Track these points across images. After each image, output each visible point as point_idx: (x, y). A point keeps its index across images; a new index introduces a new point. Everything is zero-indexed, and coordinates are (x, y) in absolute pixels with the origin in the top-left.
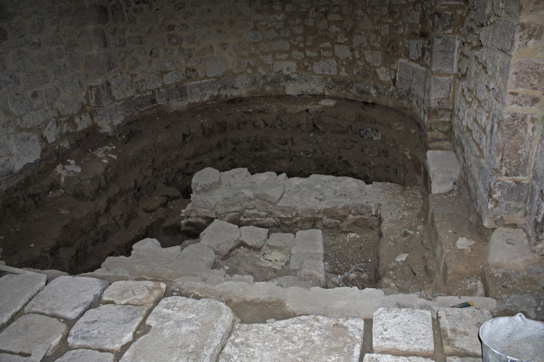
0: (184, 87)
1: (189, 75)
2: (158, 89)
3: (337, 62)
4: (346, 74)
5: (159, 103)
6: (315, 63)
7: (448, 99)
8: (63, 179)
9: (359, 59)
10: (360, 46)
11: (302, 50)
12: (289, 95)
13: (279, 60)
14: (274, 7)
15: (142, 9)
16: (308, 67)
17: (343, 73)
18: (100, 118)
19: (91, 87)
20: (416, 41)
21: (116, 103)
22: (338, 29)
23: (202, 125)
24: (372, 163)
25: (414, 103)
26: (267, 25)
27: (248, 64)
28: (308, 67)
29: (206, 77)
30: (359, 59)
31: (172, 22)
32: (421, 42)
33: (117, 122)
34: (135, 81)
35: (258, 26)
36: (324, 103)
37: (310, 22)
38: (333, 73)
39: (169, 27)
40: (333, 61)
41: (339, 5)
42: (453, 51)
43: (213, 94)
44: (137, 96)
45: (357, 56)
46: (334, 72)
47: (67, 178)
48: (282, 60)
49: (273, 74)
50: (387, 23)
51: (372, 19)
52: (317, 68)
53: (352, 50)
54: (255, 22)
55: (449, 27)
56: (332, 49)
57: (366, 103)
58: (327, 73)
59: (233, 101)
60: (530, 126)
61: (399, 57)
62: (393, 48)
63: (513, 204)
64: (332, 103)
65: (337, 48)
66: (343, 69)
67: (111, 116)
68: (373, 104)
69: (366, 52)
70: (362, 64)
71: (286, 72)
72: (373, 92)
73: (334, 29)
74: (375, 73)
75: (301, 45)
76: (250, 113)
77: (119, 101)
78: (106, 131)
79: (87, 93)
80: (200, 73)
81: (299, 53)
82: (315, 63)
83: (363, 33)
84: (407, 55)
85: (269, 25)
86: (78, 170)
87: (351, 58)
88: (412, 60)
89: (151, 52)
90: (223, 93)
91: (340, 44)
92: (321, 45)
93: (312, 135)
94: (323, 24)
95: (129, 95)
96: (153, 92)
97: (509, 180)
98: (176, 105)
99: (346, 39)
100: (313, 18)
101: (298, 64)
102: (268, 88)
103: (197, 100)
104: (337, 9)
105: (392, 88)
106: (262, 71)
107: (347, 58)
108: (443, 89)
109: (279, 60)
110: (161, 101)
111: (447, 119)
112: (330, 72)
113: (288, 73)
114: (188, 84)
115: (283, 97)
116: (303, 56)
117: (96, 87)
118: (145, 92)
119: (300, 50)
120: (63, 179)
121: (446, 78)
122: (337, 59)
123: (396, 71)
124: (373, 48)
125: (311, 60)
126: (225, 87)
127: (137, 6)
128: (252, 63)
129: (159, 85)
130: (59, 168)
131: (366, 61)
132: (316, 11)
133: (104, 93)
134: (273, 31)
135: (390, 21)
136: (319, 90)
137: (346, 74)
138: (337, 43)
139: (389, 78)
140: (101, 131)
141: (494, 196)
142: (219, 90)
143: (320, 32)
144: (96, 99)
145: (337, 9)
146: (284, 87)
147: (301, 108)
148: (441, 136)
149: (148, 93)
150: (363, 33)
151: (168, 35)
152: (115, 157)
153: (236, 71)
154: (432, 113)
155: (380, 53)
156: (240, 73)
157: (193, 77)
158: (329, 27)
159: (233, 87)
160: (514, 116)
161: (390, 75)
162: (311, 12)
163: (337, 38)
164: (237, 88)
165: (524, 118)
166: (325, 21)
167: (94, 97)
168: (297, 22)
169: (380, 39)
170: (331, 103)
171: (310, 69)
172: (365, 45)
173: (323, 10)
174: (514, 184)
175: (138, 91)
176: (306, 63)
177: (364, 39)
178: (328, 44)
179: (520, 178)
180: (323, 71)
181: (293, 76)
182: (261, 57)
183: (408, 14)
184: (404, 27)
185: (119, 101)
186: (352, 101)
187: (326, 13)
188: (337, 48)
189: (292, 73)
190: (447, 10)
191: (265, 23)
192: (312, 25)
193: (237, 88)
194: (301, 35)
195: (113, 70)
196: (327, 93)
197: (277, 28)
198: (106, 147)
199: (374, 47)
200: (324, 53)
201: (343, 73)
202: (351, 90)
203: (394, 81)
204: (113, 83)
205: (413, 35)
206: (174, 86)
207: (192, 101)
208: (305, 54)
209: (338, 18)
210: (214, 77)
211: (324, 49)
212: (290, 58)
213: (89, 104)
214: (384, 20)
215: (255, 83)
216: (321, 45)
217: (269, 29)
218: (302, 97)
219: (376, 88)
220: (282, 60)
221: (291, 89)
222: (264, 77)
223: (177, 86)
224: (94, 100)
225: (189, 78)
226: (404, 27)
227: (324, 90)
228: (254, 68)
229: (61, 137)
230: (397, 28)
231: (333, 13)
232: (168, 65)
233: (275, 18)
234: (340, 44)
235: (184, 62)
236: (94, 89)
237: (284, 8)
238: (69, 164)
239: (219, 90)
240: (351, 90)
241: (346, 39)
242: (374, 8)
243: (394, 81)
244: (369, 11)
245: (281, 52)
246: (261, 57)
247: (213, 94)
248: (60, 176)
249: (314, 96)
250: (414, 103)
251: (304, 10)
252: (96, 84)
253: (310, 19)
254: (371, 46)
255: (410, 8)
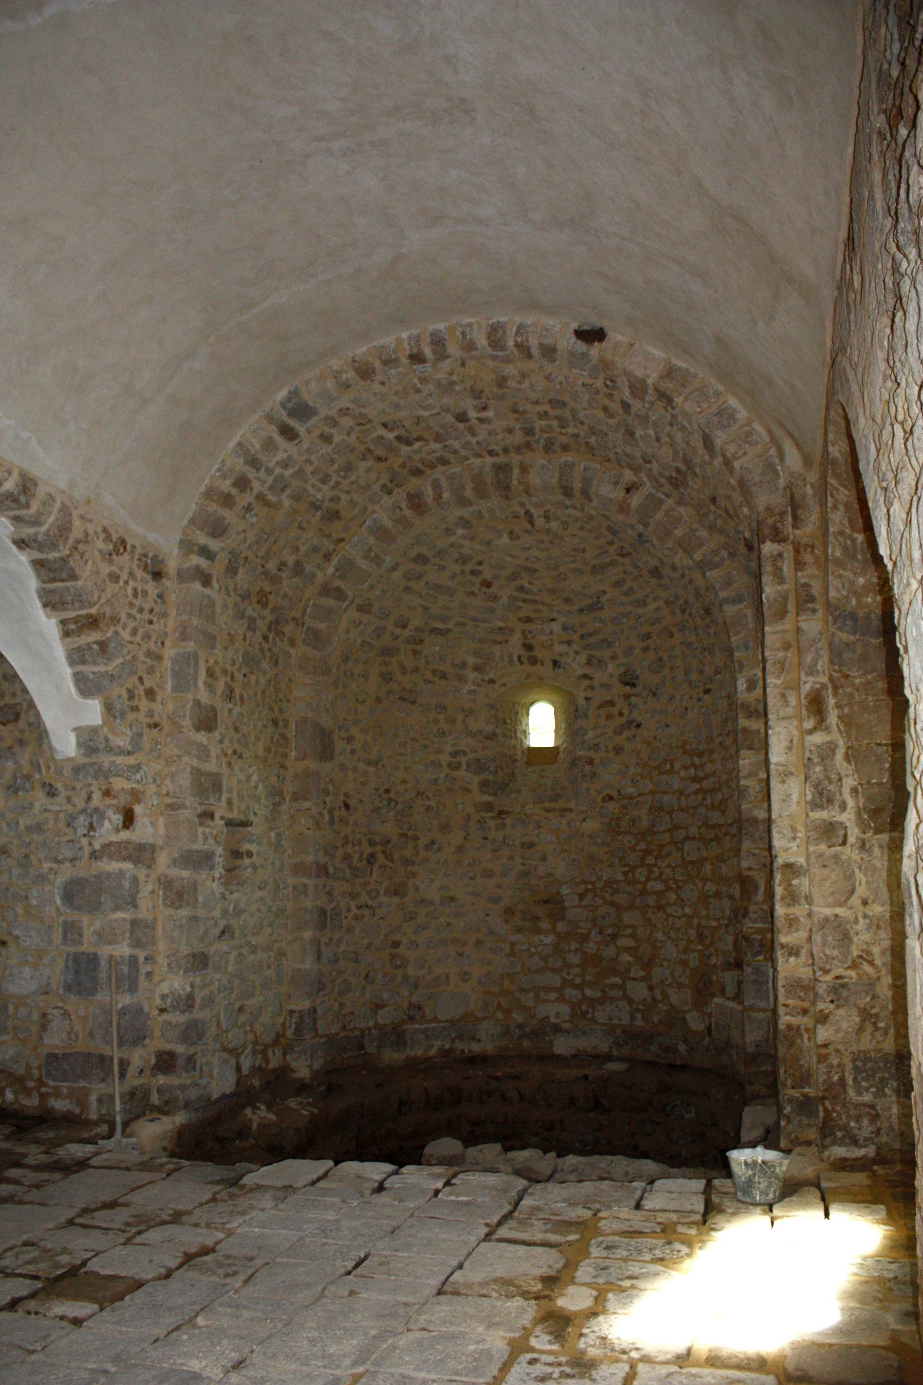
0: (405, 1031)
1: (412, 1013)
2: (369, 1029)
3: (630, 1006)
4: (643, 1024)
5: (368, 1050)
6: (598, 1007)
7: (767, 1041)
8: (255, 1125)
9: (661, 1001)
10: (662, 982)
11: (580, 987)
12: (558, 1056)
13: (545, 1001)
14: (540, 924)
15: (363, 916)
16: (587, 1012)
17: (639, 1022)
18: (295, 1056)
19: (292, 1012)
20: (731, 973)
21: (318, 1039)
22: (630, 959)
23: (426, 1090)
24: (684, 1153)
25: (735, 1057)
26: (529, 950)
27: (499, 1004)
28: (587, 1012)
29: (435, 1019)
30: (661, 1001)
31: (397, 937)
32: (736, 973)
33: (317, 1065)
34: (343, 1012)
35: (516, 950)
36: (610, 1066)
37: (591, 948)
38: (623, 1023)
39: (394, 942)
40: (624, 1004)
41: (632, 926)
42: (75, 610)
43: (443, 1046)
44: (342, 1034)
45: (659, 996)
46: (626, 1021)
47: (259, 1124)
48: (549, 1001)
49: (534, 1022)
50: (695, 951)
51: (677, 946)
52: (601, 1015)
53: (651, 988)
54: (513, 944)
55: (759, 953)
56: (622, 987)
57: (673, 1066)
58: (616, 1022)
59: (472, 1060)
60: (806, 1036)
61: (713, 995)
62: (705, 984)
63: (805, 1120)
64: (621, 1066)
65: (629, 985)
66: (639, 1015)
67: (312, 1055)
68: (684, 1067)
69: (670, 991)
70: (665, 1008)
71: (553, 1020)
72: (682, 1048)
73: (626, 958)
74: (684, 1020)
75: (578, 981)
76: (498, 1078)
77: (322, 1036)
78: (301, 1075)
79: (285, 1019)
80: (427, 1013)
81: (574, 992)
82: (598, 1007)
83: (665, 964)
84: (723, 992)
85: (533, 950)
86: (273, 1117)
87: (649, 1000)
88: (728, 999)
89: (367, 976)
90: (459, 1045)
91: (634, 979)
92: (608, 982)
93: (592, 1115)
94: (610, 951)
95: (333, 1031)
96: (363, 1032)
97: (796, 1093)
98: (390, 1056)
99: (643, 973)
100: (596, 943)
101: (572, 1008)
102: (526, 1043)
103: (419, 1053)
104: (629, 931)
105: (707, 1040)
106: (518, 1017)
107: (645, 999)
108: (759, 1028)
109: (545, 1001)
110: (371, 1048)
111: (770, 1069)
112: (620, 1020)
113: (557, 1021)
114: (409, 1027)
115: (550, 1058)
116: (580, 996)
117: (300, 1012)
118: (352, 1030)
119: (575, 987)
120: (255, 1125)
121: (762, 1015)
122: (630, 1001)
123: (710, 1015)
124: (680, 985)
125: (591, 1002)
126: (461, 1038)
127: (358, 912)
128: (504, 1001)
129: (371, 1024)
130: (248, 1111)
131: (670, 1004)
132: (600, 933)
133: (308, 1020)
134: (537, 958)
135: (700, 947)
136: (604, 1046)
137: (643, 1024)
138: (630, 978)
139: (702, 1027)
140: (295, 1076)
141: (785, 1112)
142: (453, 1040)
143: (605, 962)
144: (296, 1029)
145: (629, 931)
146: (551, 1043)
147: (575, 1073)
148: (764, 1091)
149: (356, 1032)
150: (665, 964)
151: (391, 954)
152: (316, 1111)
153: (479, 1015)
154: (752, 1059)
155: (688, 991)
156: (484, 1018)
157: (418, 1017)
158: (618, 955)
159: (473, 1038)
160: (789, 1027)
161: (704, 1021)
162: (592, 934)
163: (629, 971)
164: (479, 1041)
165: (798, 1028)
166: (612, 948)
167: (293, 1026)
168: (573, 948)
169: (688, 972)
170: (621, 1066)
171: (589, 1016)
172: (670, 980)
173: (610, 931)
174: (801, 1098)
175: (344, 1028)
176: (584, 1008)
177: (667, 972)
178: (617, 980)
179: (807, 1090)
180: (610, 1019)
181: (566, 1026)
182: (517, 995)
183: (720, 939)
184: (717, 955)
185: (322, 1036)
186: (653, 1063)
187: (614, 937)
188: (629, 985)
189: (564, 1021)
190: (754, 933)
191: (526, 947)
192: (594, 952)
193: (479, 1041)
194: (578, 966)
195: (322, 993)
196: (615, 1053)
197: (543, 954)
198: (300, 1099)
199: (681, 983)
200: (612, 993)
201: (639, 1022)
202: (651, 1048)
203: (709, 1029)
204: (319, 1012)
205: (727, 966)
206: (390, 1028)
207: (412, 1053)
208: (584, 994)
209: (631, 943)
210: (447, 1021)
211: (612, 986)
212: (561, 999)
213: (283, 1035)
214: (692, 947)
215: (506, 1033)
216: (608, 982)
217: (532, 955)
218: (577, 1058)
219: (685, 1041)
220: (549, 1001)
221: (562, 1046)
222: (521, 1026)
223: (394, 1029)
224: (292, 1030)
225: (412, 1018)
226: (717, 955)
227: (611, 1048)
228: (507, 1012)
229: (256, 1070)
230: (708, 957)
231: (624, 936)
232: (386, 996)
233: (541, 941)
234: (634, 979)
235: (407, 994)
236: (297, 1015)
237: (554, 927)
238: (259, 1109)
239: (453, 1040)
240: (651, 1048)
241: (643, 973)
242: (679, 930)
243: (709, 1029)
244: (672, 934)
245: (548, 989)
246: (517, 995)
247: (443, 1046)
248: (251, 1121)
249: (596, 1057)
250: (735, 1057)
251: (584, 931)
252: (301, 1008)
253: (591, 945)
254: (677, 983)
255: (722, 931)
